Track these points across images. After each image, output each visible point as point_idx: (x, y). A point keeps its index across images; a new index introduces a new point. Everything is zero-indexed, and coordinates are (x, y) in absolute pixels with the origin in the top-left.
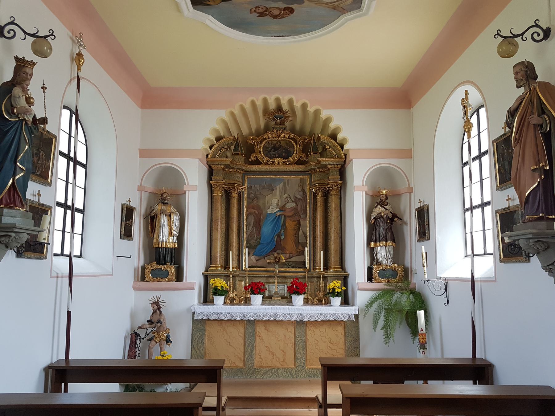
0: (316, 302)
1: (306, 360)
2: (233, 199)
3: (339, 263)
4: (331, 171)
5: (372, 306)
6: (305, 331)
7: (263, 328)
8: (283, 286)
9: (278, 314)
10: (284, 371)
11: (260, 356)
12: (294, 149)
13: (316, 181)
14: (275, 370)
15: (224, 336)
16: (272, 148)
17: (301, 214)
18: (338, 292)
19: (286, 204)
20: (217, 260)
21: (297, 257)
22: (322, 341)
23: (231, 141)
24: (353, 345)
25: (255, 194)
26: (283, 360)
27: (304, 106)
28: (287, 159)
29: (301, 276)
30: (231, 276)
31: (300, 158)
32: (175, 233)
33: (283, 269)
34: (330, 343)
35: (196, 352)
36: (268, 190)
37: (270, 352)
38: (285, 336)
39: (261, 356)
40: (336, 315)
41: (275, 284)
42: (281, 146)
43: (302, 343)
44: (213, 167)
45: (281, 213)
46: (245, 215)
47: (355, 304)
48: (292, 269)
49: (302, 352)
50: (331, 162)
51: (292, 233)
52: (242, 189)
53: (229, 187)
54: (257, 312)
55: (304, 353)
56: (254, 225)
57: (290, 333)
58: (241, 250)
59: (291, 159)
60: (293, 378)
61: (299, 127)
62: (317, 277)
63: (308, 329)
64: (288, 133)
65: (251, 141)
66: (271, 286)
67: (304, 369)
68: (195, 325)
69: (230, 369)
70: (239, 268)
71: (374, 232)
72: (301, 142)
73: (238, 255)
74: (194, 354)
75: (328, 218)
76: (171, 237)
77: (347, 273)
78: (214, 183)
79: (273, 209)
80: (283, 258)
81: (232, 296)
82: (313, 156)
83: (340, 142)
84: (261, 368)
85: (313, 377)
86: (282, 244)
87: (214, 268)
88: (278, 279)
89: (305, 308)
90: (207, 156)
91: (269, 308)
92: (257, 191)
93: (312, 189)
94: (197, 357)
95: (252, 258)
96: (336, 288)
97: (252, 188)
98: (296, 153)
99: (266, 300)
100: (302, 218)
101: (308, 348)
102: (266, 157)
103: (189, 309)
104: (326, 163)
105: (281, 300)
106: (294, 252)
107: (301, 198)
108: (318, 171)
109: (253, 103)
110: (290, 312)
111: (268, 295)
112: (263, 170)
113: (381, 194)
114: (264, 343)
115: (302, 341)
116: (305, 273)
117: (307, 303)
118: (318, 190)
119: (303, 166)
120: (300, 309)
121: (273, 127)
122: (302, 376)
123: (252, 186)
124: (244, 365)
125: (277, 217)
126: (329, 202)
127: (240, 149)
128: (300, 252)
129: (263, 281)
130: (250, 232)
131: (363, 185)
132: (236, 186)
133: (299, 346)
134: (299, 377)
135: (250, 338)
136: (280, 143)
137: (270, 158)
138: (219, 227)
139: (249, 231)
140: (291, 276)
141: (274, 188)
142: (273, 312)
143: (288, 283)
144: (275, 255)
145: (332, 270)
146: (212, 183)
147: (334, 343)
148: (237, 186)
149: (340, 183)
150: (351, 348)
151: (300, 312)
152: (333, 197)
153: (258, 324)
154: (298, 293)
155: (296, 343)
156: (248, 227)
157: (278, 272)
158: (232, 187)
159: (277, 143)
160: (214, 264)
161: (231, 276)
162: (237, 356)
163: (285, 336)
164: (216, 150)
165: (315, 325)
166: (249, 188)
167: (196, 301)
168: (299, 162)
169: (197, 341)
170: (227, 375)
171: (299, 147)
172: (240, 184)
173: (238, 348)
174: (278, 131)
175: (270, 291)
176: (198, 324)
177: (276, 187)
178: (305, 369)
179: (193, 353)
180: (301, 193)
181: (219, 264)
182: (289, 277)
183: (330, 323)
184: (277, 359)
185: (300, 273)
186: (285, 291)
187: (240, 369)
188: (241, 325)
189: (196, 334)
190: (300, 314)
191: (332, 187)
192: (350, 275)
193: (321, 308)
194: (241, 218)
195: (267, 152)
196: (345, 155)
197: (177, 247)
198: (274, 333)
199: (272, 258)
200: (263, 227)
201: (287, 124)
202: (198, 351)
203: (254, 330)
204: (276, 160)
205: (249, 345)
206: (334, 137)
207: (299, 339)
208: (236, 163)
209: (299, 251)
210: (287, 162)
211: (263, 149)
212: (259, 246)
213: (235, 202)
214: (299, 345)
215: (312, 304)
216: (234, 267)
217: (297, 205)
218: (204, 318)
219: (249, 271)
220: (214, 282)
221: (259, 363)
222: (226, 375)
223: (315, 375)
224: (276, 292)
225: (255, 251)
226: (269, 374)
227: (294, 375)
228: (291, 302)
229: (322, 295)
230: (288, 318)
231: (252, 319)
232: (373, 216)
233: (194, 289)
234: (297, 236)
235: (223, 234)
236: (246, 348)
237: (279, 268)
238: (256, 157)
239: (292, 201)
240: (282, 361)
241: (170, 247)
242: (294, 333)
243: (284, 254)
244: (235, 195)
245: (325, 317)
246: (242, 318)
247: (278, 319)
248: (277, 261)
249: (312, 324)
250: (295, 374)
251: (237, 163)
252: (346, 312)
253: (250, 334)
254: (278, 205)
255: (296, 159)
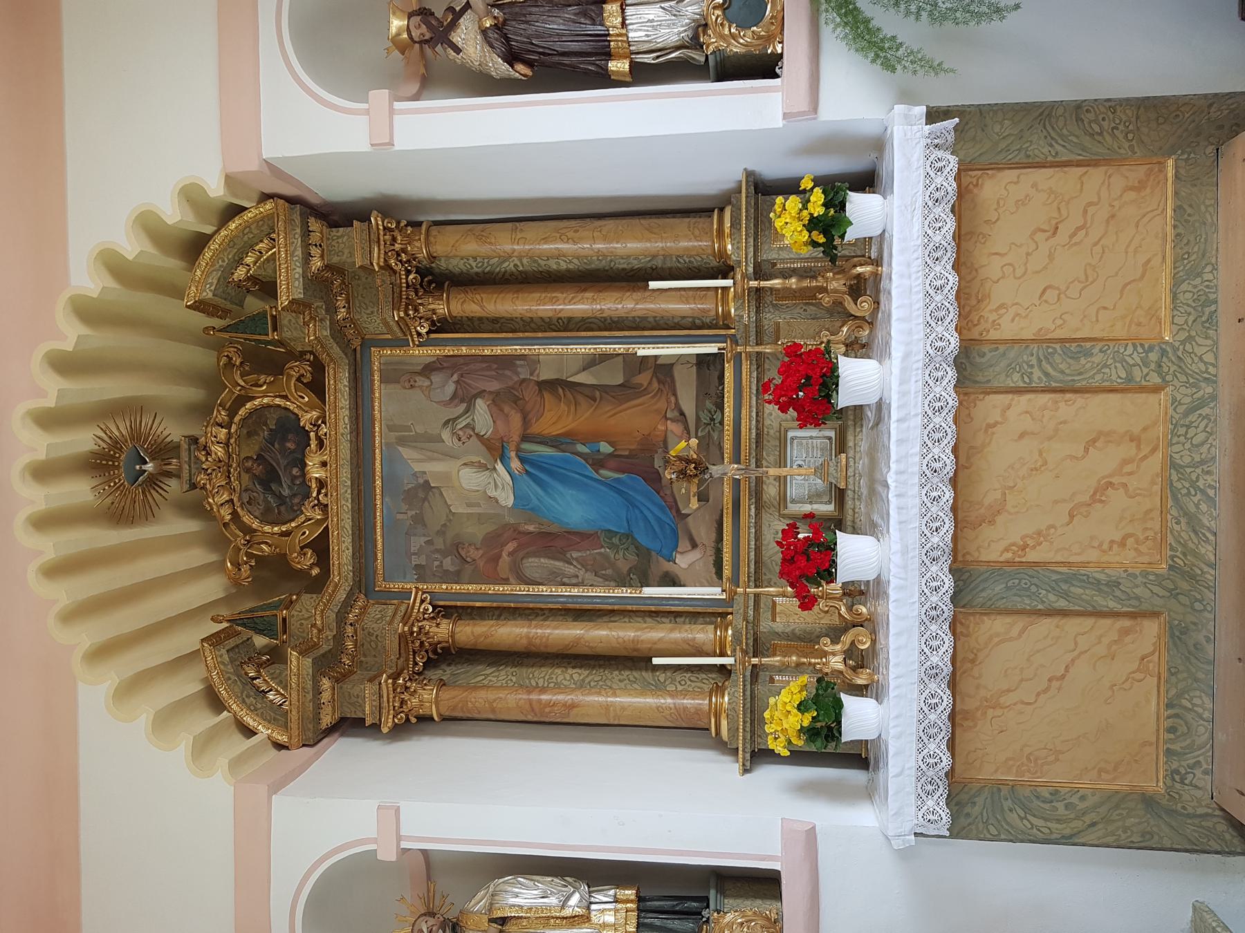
0: (863, 307)
1: (1136, 342)
2: (457, 636)
3: (700, 217)
4: (335, 260)
5: (893, 39)
6: (1002, 348)
7: (987, 532)
8: (792, 443)
9: (925, 467)
10: (1182, 439)
11: (1115, 546)
12: (269, 406)
13: (386, 324)
14: (1179, 479)
15: (1023, 703)
16: (267, 488)
17: (516, 379)
18: (826, 205)
19: (477, 434)
20: (692, 710)
21: (679, 393)
22: (1045, 268)
23: (224, 651)
24: (1065, 131)
25: (445, 554)
26: (1134, 444)
27: (64, 365)
28: (308, 432)
29: (755, 374)
30: (755, 661)
31: (302, 382)
32: (575, 899)
33: (728, 445)
34: (1055, 233)
35: (1093, 824)
36: (426, 503)
37: (1095, 502)
38: (1022, 435)
39: (1112, 542)
40: (930, 203)
41: (785, 477)
42: (260, 456)
43: (1057, 359)
44: (327, 720)
45: (513, 454)
46: (522, 590)
47: (872, 130)
48: (727, 410)
49: (1098, 358)
50: (292, 255)
51: (589, 413)
52: (422, 601)
53: (414, 652)
54: (917, 561)
55: (1101, 351)
56: (560, 555)
57: (1008, 413)
58: (653, 608)
59: (307, 418)
60: (1214, 397)
61: (193, 390)
62: (758, 308)
63: (994, 335)
64: (209, 429)
65: (245, 568)
66: (793, 491)
67: (1175, 350)
68: (973, 827)
69: (1174, 679)
70: (724, 615)
71: (566, 60)
72: (244, 381)
73: (675, 617)
74: (1100, 833)
75: (525, 272)
76: (594, 919)
77: (741, 181)
78: (391, 717)
79: (496, 486)
80: (682, 446)
81: (839, 658)
82: (287, 334)
83: (215, 221)
84: (1170, 539)
85: (1213, 308)
86: (631, 450)
87: (724, 723)
88: (764, 463)
89: (897, 350)
90: (280, 746)
91: (900, 508)
92: (433, 544)
93: (419, 334)
94: (1114, 821)
95: (684, 566)
96: (805, 213)
97: (424, 563)
98: (285, 397)
99: (850, 512)
100: (531, 374)
101: (1078, 330)
102: (302, 513)
103: (904, 855)
104: (297, 276)
105: (851, 453)
106: (662, 405)
107: (455, 377)
108: (349, 313)
109: (58, 570)
110: (916, 415)
111: (831, 503)
112: (348, 524)
113: (405, 36)
114: (1052, 526)
115: (1046, 358)
116: (743, 355)
117: (863, 346)
118: (416, 310)
119: (330, 371)
120: (903, 370)
121: (186, 487)
122: (1209, 358)
123: (414, 563)
124: (1155, 614)
125: (526, 470)
126: (464, 269)
127: (268, 613)
128: (659, 382)
129: (775, 527)
130: (587, 570)
131: (367, 112)
132: (406, 629)
133: (1067, 371)
134: (1211, 369)
135: (1034, 589)
136: (247, 458)
137: (307, 495)
138: (560, 697)
139: (581, 573)
140: (754, 414)
141: (421, 481)
142: (917, 488)
143: (781, 425)
144: (669, 475)
145: (729, 247)
146: (390, 724)
147: (1056, 215)
148: (411, 621)
149: (380, 223)
150: (1077, 137)
151: (915, 366)
152: (439, 249)
153: (968, 553)
154: (828, 379)
155: (1054, 384)
156: (565, 580)
157: (739, 463)
158: (413, 642)
159: (248, 470)
160: (706, 721)
161: (755, 661)
162: (1114, 647)
163: (1022, 435)
164: (259, 712)
165: (974, 302)
166: (422, 574)
167: (863, 817)
168: (317, 387)
169: (1046, 820)
170: (1198, 693)
171: (261, 386)
172: (403, 608)
173: (1076, 643)
174: (204, 467)
175: (814, 497)
176: (968, 815)
177: (415, 474)
178: (1177, 344)
179: (1099, 838)
180: (437, 378)
181: (707, 702)
182: (757, 421)
183: (966, 234)
184: (1128, 469)
185: (744, 381)
186: (811, 438)
187: (1172, 636)
188: (971, 629)
189: (1012, 827)
190: (926, 366)
191: (398, 255)
192: (751, 168)
193: (902, 276)
194: (531, 605)
195: (283, 508)
196: (265, 197)
197: (634, 892)
198: (1012, 485)
199: (682, 489)
200: (568, 524)
201: (174, 431)
202: (1088, 819)
203: (999, 570)
204: (315, 473)
205: (1065, 595)
206: (194, 246)
207: (1037, 373)
208: (315, 631)
209: (655, 385)
210: (320, 433)
211: (273, 523)
212: (636, 536)
213: (469, 632)
214: (1062, 372)
215: (871, 323)
216: (720, 637)
217: (481, 394)
218: (942, 791)
219: (735, 581)
220: (782, 738)
221: (1143, 548)
222: (1200, 697)
223: (1203, 298)
224: (820, 471)
225: (659, 553)
226: (1197, 506)
227: (1201, 393)
228: (858, 410)
229: (833, 279)
230: (945, 421)
231: (948, 582)
232: (498, 67)
233: (814, 828)
234: (598, 394)
235: (590, 677)
236: (1077, 608)
237: (723, 463)
238: (302, 548)
239: (467, 411)
240: (1138, 447)
241: (635, 921)
242: (1010, 396)
243: (670, 440)
244: (442, 630)
245: (939, 254)
246: (946, 627)
247: (948, 468)
248: (694, 469)
249: (970, 312)
250: (1199, 389)
251: (314, 625)
252: (918, 160)
253: (1014, 591)
254: (482, 467)
255: (307, 399)
